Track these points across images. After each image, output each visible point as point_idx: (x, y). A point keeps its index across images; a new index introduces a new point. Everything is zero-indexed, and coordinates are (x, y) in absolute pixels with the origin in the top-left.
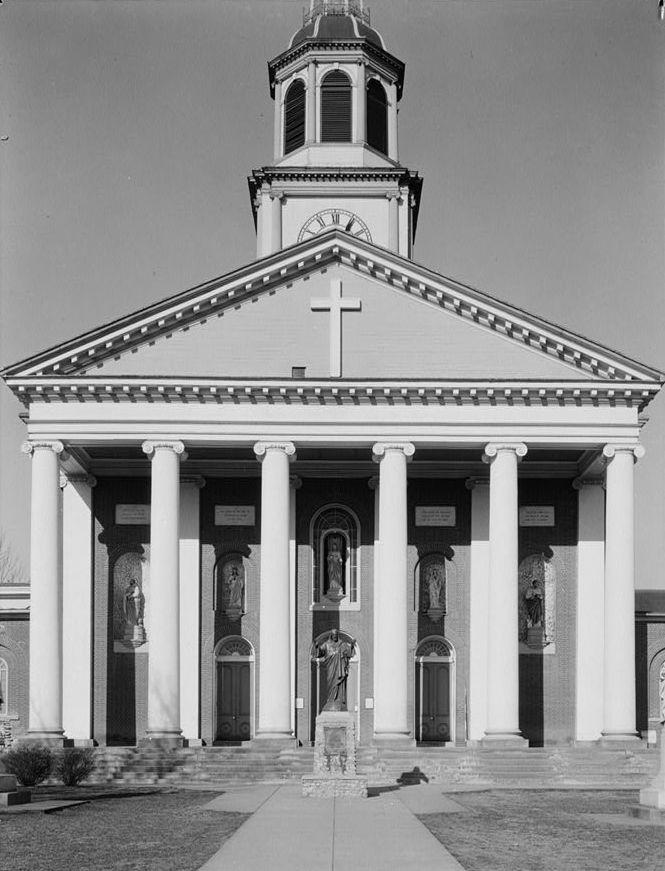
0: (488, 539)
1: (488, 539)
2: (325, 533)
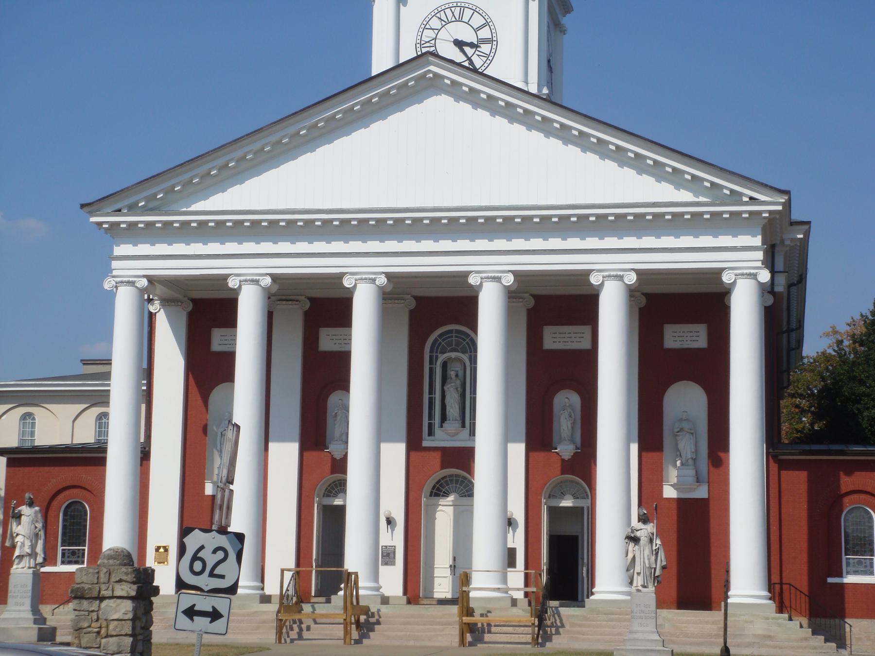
0: (208, 577)
1: (208, 577)
2: (442, 358)
